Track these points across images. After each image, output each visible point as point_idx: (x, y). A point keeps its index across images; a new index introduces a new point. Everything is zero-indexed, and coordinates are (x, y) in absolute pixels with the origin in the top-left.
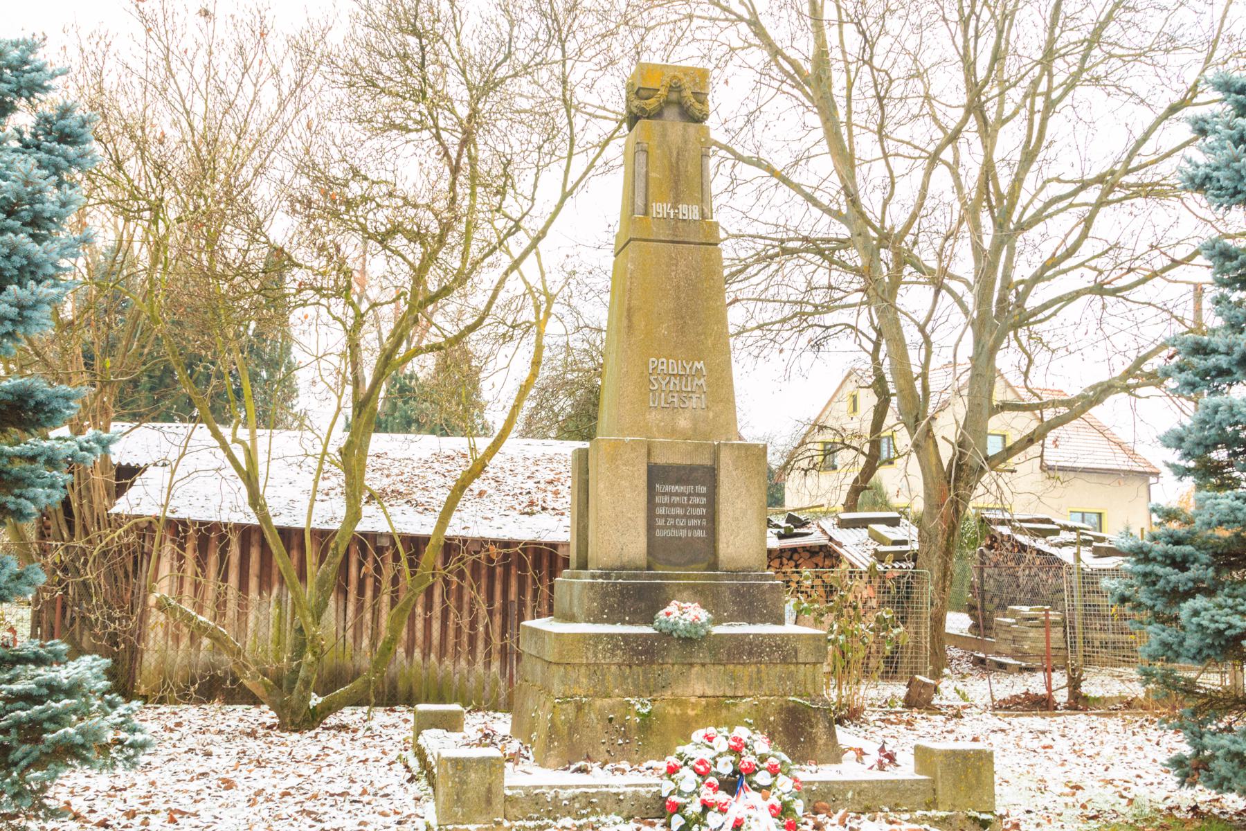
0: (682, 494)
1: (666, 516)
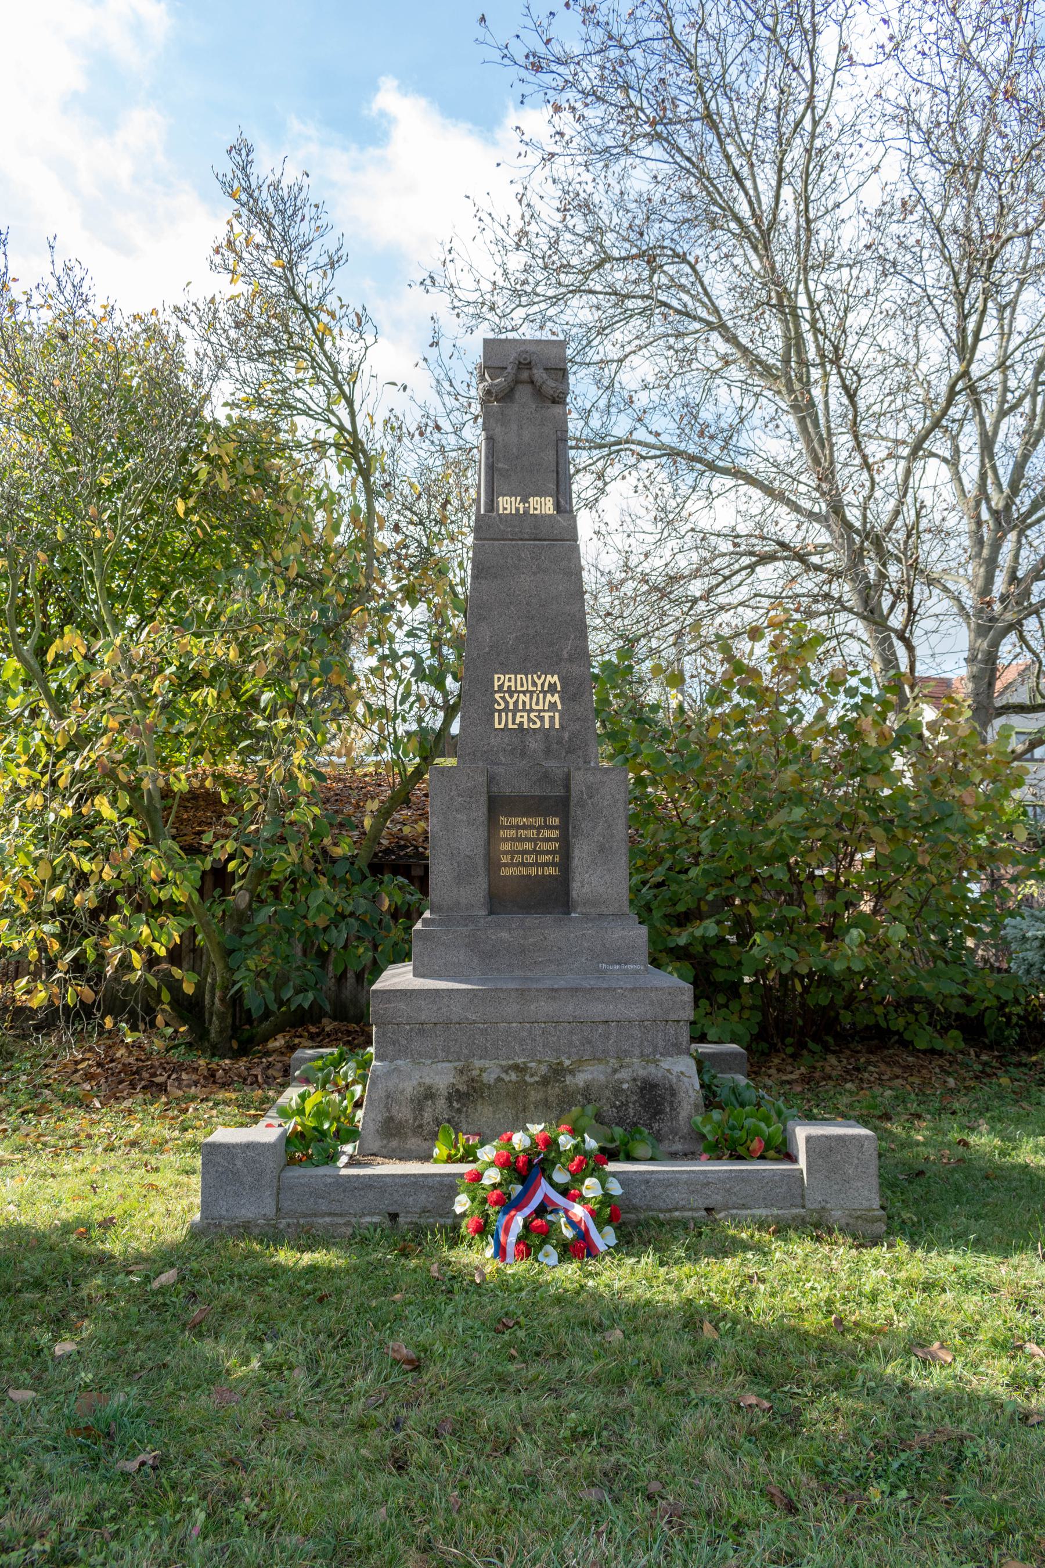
0: (532, 827)
1: (513, 853)
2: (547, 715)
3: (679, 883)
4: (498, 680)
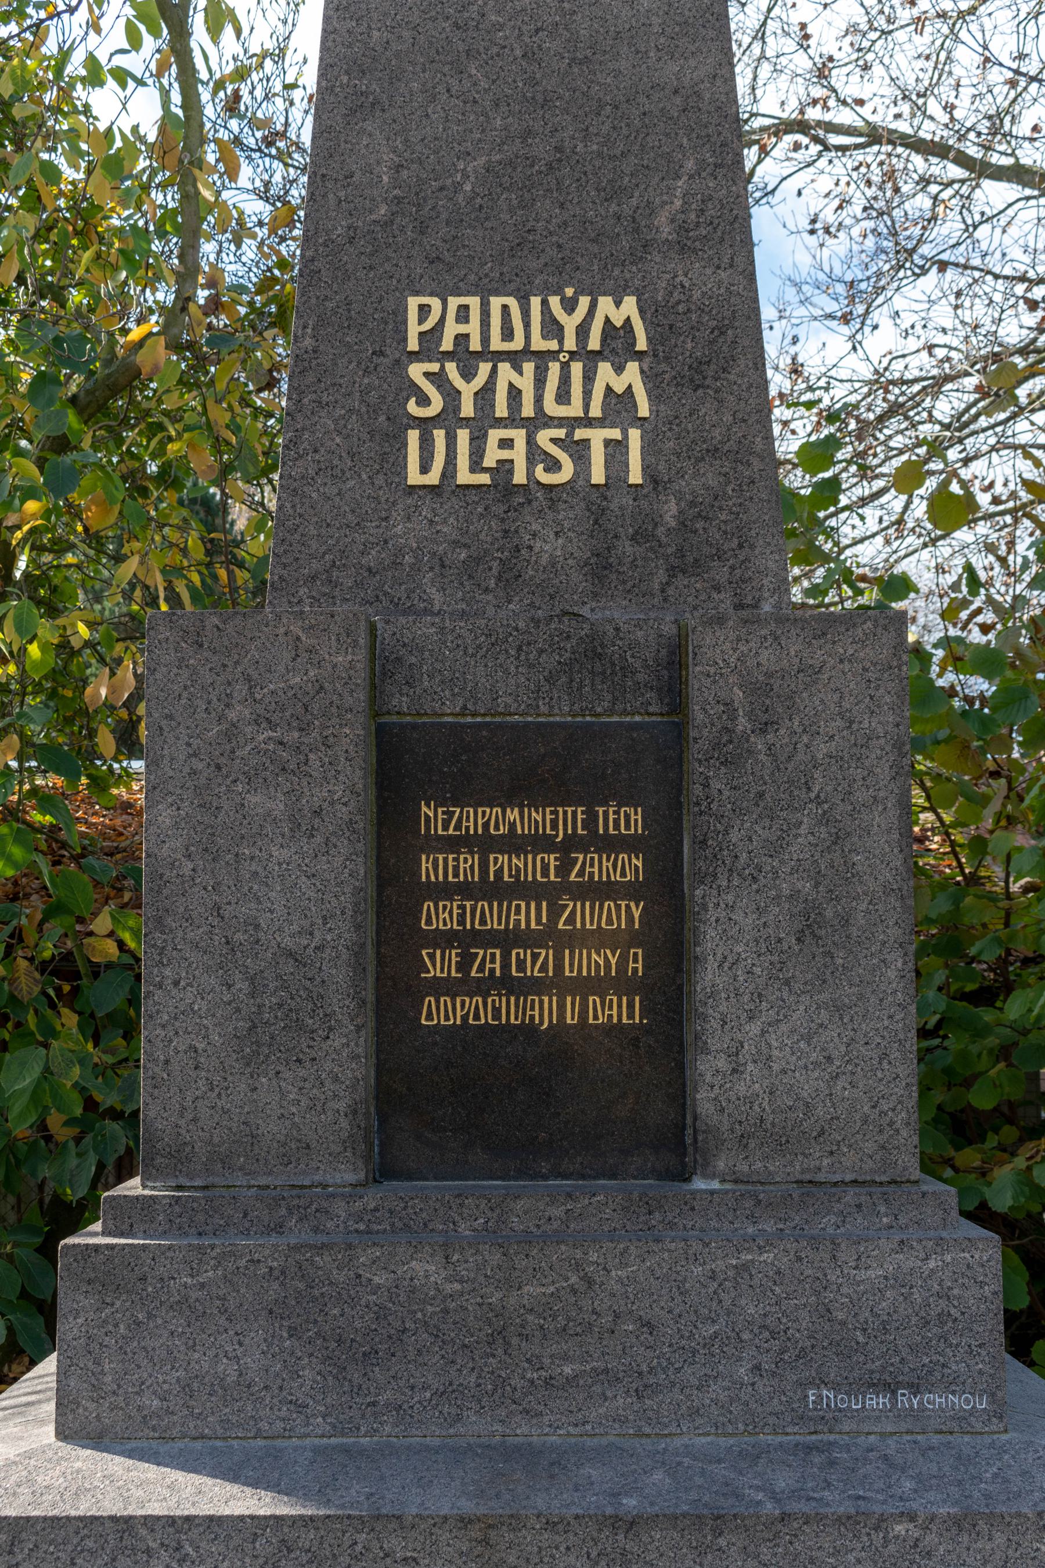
0: (540, 843)
1: (466, 940)
2: (597, 437)
3: (980, 1032)
4: (419, 313)
